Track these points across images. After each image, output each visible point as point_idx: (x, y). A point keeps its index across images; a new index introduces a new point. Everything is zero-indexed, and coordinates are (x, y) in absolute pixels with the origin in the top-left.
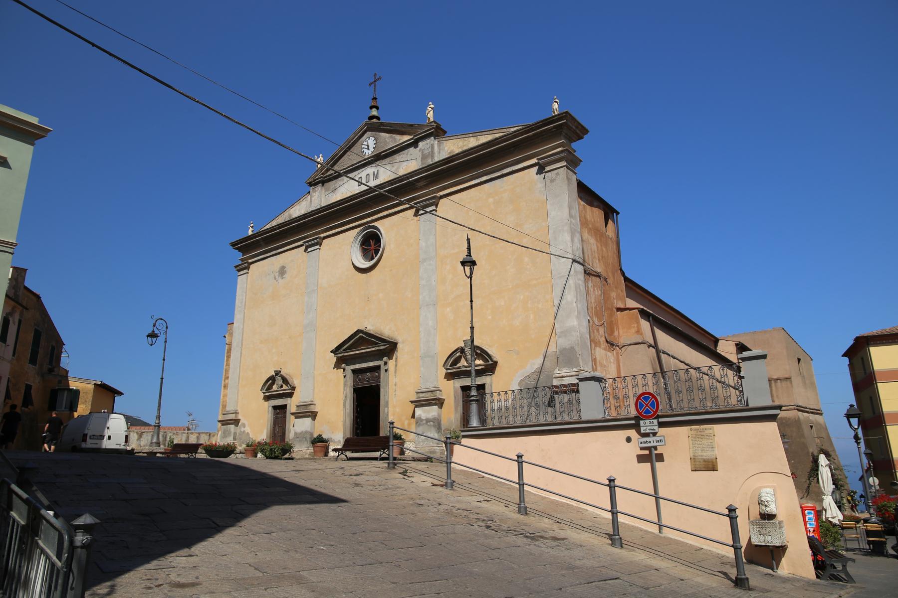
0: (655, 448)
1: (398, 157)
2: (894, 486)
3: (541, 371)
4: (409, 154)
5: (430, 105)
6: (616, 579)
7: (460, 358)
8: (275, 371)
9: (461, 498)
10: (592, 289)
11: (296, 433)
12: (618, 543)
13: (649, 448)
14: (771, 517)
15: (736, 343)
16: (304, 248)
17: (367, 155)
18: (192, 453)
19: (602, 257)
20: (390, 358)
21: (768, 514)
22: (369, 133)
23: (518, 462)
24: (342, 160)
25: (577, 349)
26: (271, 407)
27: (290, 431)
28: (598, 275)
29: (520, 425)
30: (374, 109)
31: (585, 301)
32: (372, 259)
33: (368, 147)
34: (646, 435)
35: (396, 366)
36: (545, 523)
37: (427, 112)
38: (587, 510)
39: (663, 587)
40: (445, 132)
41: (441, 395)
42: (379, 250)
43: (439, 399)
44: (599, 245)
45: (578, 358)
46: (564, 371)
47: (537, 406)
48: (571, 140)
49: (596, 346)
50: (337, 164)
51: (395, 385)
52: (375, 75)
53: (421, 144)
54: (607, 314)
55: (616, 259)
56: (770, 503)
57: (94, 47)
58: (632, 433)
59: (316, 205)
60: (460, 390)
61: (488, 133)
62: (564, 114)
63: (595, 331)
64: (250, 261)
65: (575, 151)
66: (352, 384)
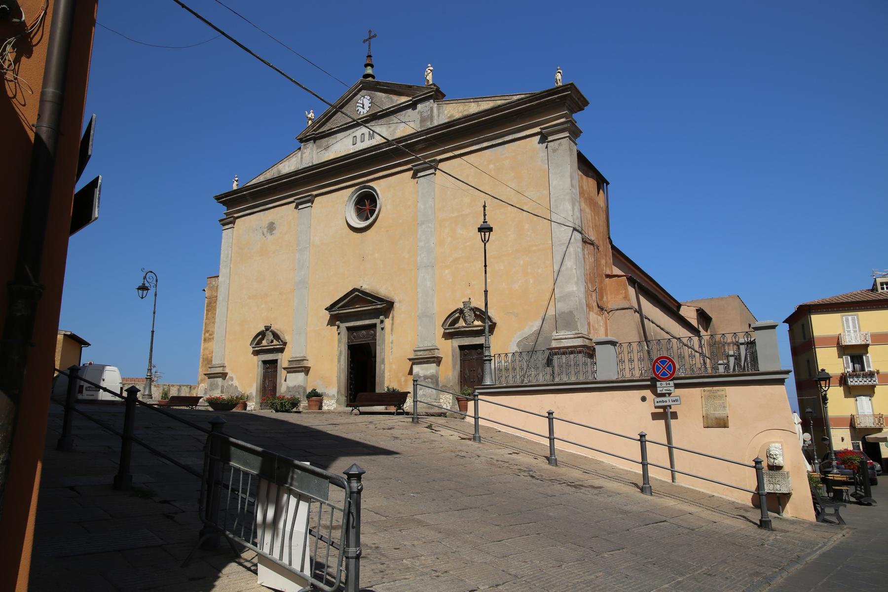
0: (670, 407)
1: (394, 119)
2: (825, 441)
3: (539, 332)
4: (407, 115)
5: (429, 67)
6: (664, 521)
7: (458, 318)
8: (265, 327)
9: (493, 450)
10: (587, 257)
11: (288, 388)
12: (648, 491)
13: (664, 407)
14: (779, 468)
15: (697, 308)
16: (294, 204)
17: (362, 113)
18: (192, 406)
19: (595, 226)
20: (387, 317)
21: (776, 466)
22: (363, 92)
23: (475, 419)
24: (335, 117)
25: (575, 313)
26: (261, 362)
27: (282, 385)
28: (592, 244)
29: (512, 385)
30: (369, 67)
31: (583, 269)
32: (367, 219)
33: (363, 106)
34: (663, 395)
35: (393, 324)
36: (576, 474)
37: (426, 74)
38: (603, 462)
39: (704, 528)
40: (444, 96)
41: (439, 353)
42: (375, 210)
43: (438, 358)
44: (593, 214)
45: (577, 322)
46: (562, 334)
47: (537, 368)
48: (573, 111)
49: (590, 311)
50: (330, 121)
51: (392, 343)
52: (370, 31)
53: (419, 106)
54: (599, 280)
55: (606, 228)
56: (778, 456)
57: (184, 8)
58: (647, 393)
59: (307, 163)
60: (458, 350)
61: (489, 99)
62: (569, 86)
63: (590, 297)
64: (236, 215)
65: (576, 122)
66: (347, 341)
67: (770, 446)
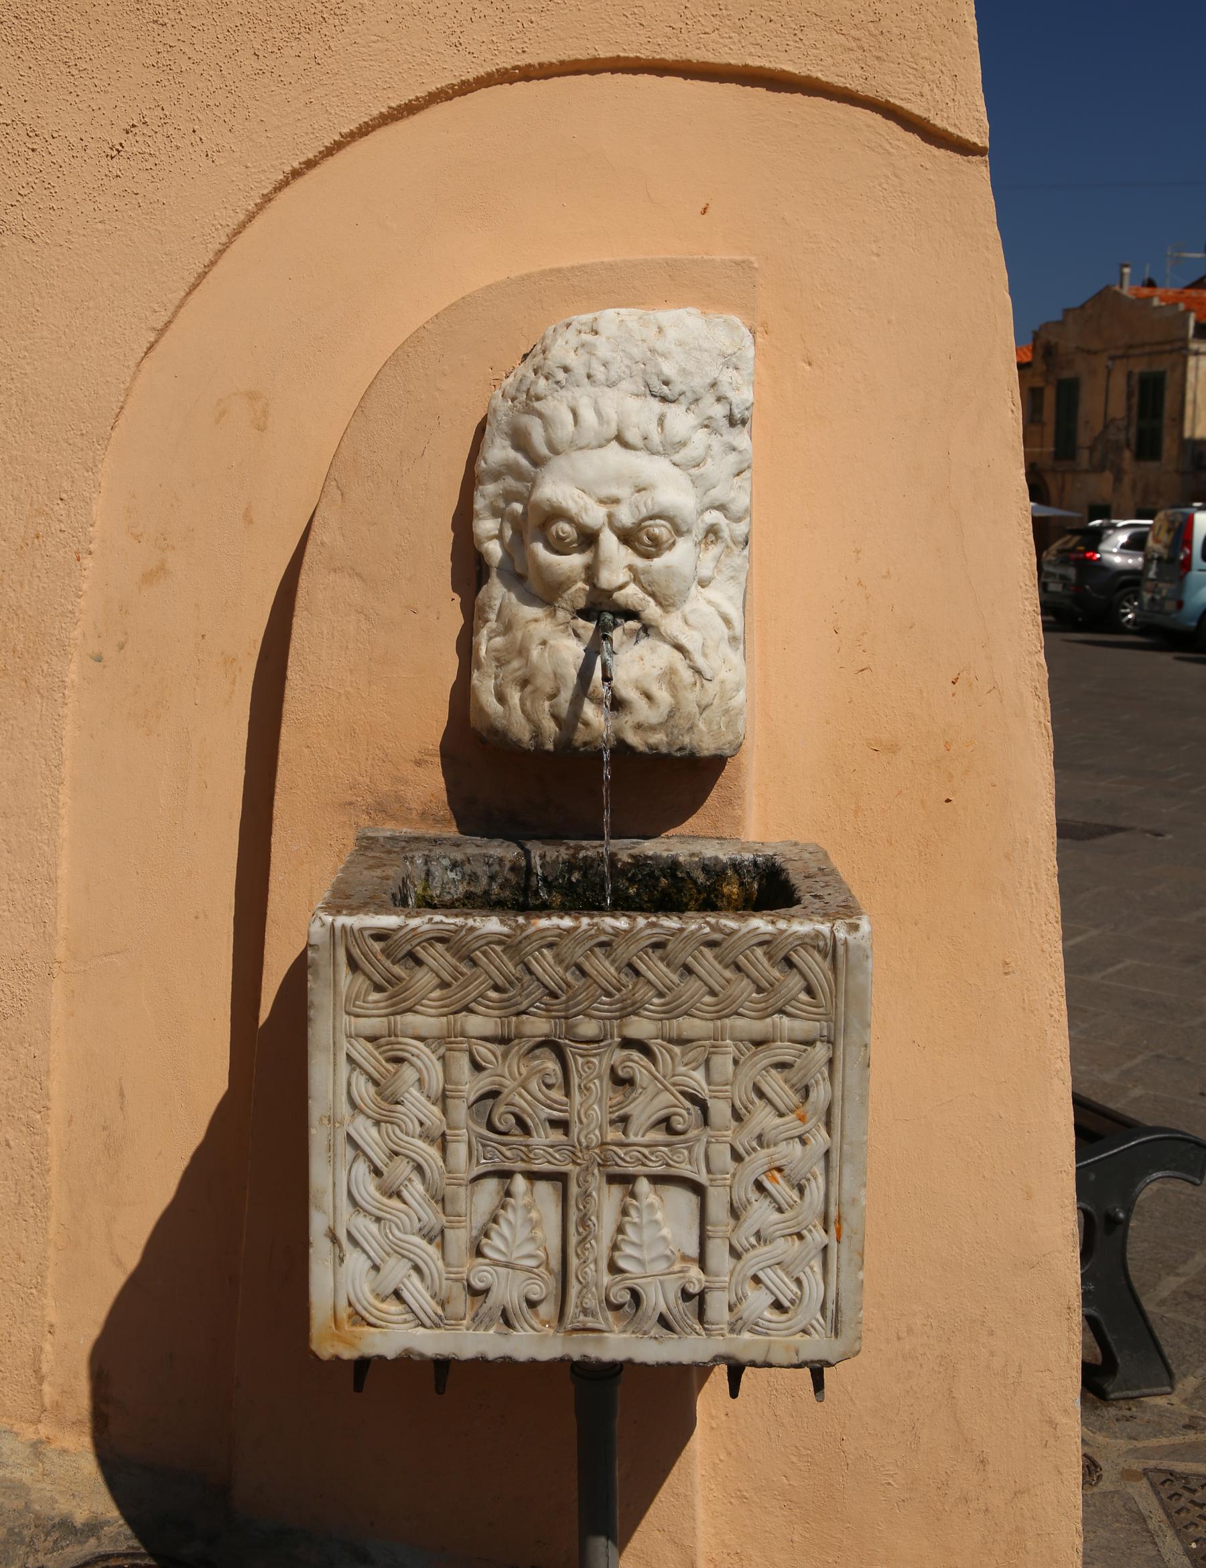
67: (563, 350)
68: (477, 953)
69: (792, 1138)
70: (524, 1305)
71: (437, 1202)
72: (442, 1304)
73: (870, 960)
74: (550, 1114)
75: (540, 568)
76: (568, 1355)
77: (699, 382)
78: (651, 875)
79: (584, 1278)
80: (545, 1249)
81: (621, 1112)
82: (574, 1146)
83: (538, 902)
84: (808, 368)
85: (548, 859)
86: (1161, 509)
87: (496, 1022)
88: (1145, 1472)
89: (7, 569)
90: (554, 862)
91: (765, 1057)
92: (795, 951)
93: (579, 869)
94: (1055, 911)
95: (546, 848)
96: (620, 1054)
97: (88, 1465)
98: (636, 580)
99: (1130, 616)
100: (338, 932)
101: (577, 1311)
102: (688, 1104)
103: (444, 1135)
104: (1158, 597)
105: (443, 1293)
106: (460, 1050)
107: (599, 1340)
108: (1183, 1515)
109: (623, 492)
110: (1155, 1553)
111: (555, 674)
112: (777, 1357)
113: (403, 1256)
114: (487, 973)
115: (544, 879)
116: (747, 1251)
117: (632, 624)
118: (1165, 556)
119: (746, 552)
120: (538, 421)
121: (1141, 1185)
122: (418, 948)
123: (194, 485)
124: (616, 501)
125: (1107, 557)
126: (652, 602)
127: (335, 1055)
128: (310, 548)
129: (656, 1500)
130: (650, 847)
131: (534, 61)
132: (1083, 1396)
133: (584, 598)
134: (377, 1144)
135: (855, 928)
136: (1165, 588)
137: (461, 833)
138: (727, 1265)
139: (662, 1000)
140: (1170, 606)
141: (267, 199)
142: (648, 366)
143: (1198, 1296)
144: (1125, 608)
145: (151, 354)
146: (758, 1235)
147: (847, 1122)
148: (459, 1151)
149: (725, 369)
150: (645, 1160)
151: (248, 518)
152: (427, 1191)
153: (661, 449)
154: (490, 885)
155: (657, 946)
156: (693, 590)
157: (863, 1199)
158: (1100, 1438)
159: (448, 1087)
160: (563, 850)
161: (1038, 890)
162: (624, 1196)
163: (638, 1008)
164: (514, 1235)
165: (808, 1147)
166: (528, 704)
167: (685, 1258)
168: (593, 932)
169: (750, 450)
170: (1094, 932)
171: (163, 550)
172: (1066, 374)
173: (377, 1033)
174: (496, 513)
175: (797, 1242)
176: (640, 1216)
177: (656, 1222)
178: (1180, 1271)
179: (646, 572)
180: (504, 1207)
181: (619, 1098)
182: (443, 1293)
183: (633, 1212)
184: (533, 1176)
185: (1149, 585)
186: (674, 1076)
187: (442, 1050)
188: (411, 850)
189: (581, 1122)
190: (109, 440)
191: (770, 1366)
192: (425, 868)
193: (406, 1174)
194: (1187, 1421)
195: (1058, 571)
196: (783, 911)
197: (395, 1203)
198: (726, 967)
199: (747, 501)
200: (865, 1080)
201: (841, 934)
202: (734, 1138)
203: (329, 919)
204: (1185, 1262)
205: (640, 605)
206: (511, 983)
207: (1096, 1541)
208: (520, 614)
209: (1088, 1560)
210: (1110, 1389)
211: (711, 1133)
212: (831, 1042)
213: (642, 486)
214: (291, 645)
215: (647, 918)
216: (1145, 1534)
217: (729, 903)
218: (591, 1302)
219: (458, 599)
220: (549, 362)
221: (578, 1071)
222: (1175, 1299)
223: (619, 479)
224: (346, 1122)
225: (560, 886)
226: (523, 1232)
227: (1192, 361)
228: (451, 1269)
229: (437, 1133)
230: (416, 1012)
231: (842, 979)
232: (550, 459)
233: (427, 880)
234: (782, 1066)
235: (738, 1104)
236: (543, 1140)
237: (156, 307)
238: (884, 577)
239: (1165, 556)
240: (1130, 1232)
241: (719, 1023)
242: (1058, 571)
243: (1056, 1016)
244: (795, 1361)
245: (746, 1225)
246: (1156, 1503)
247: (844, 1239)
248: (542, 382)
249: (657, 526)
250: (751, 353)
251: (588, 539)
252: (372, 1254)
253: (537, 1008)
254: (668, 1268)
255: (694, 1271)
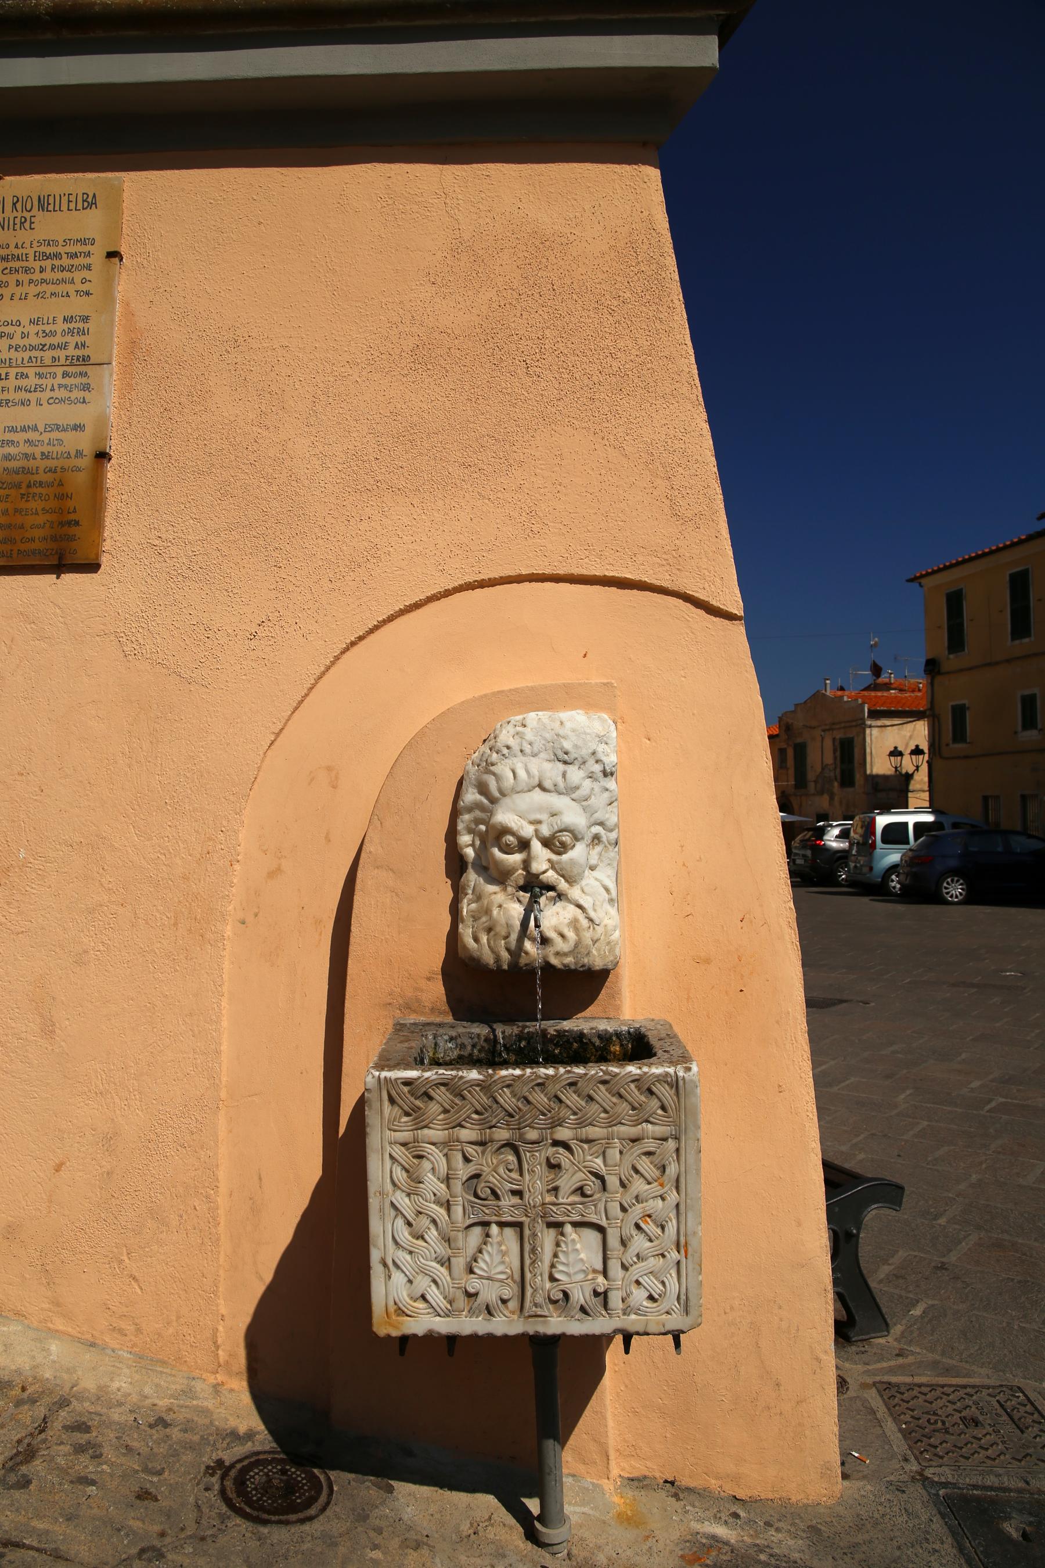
56: (578, 853)
67: (506, 736)
68: (465, 1091)
69: (656, 1197)
70: (499, 1302)
71: (445, 1241)
72: (451, 1303)
73: (698, 1088)
74: (511, 1187)
75: (497, 863)
76: (527, 1332)
77: (585, 752)
78: (568, 1041)
79: (534, 1285)
80: (511, 1268)
81: (554, 1185)
82: (526, 1206)
83: (501, 1060)
84: (648, 742)
85: (506, 1034)
86: (858, 814)
87: (477, 1133)
88: (874, 1384)
89: (191, 872)
90: (510, 1035)
91: (638, 1149)
92: (654, 1085)
93: (525, 1039)
94: (807, 1054)
95: (505, 1027)
96: (551, 1150)
97: (246, 1398)
98: (553, 868)
99: (843, 877)
100: (382, 1082)
101: (531, 1305)
102: (593, 1179)
103: (448, 1201)
104: (858, 865)
105: (451, 1296)
106: (457, 1150)
107: (545, 1322)
108: (897, 1408)
109: (543, 817)
110: (881, 1432)
111: (507, 924)
112: (651, 1329)
113: (426, 1274)
114: (471, 1104)
115: (505, 1046)
116: (632, 1265)
117: (551, 894)
118: (861, 842)
119: (616, 849)
120: (493, 778)
121: (865, 1213)
122: (430, 1090)
123: (296, 821)
124: (540, 822)
125: (828, 843)
126: (563, 880)
127: (382, 1154)
128: (363, 855)
129: (583, 1416)
130: (567, 1025)
131: (486, 577)
132: (836, 1341)
133: (523, 879)
134: (408, 1207)
135: (689, 1069)
136: (862, 860)
137: (455, 1020)
138: (620, 1274)
139: (576, 1117)
140: (865, 870)
141: (337, 658)
142: (555, 745)
143: (901, 1277)
144: (840, 872)
145: (272, 747)
146: (638, 1256)
147: (689, 1186)
148: (458, 1211)
149: (600, 744)
150: (568, 1213)
151: (328, 839)
152: (439, 1235)
153: (564, 791)
154: (472, 1050)
155: (572, 1084)
156: (586, 872)
157: (700, 1232)
158: (847, 1365)
159: (450, 1172)
160: (515, 1028)
161: (796, 1041)
162: (557, 1235)
163: (563, 1122)
164: (492, 1260)
165: (666, 1202)
166: (492, 942)
167: (595, 1271)
168: (533, 1077)
169: (616, 790)
170: (832, 1063)
171: (279, 858)
172: (799, 740)
173: (407, 1141)
174: (470, 831)
175: (661, 1259)
176: (567, 1247)
177: (577, 1250)
178: (890, 1262)
179: (559, 863)
180: (485, 1244)
181: (552, 1176)
182: (451, 1296)
183: (563, 1245)
184: (502, 1225)
185: (853, 858)
186: (584, 1162)
187: (445, 1151)
188: (425, 1031)
189: (530, 1191)
190: (248, 796)
191: (648, 1334)
192: (434, 1041)
193: (426, 1225)
194: (897, 1352)
195: (801, 852)
196: (646, 1061)
197: (420, 1242)
198: (613, 1095)
199: (616, 819)
200: (698, 1160)
201: (681, 1074)
202: (621, 1198)
203: (377, 1073)
204: (893, 1257)
205: (556, 882)
206: (486, 1109)
207: (847, 1427)
208: (486, 890)
209: (843, 1439)
210: (852, 1336)
211: (607, 1195)
212: (677, 1138)
213: (554, 813)
214: (353, 912)
215: (565, 1068)
216: (875, 1421)
217: (615, 1057)
218: (539, 1299)
219: (450, 882)
220: (498, 744)
221: (527, 1161)
222: (888, 1279)
223: (540, 809)
224: (390, 1195)
225: (514, 1050)
226: (497, 1259)
227: (868, 731)
228: (455, 1282)
229: (444, 1200)
230: (429, 1128)
231: (682, 1100)
232: (500, 799)
233: (435, 1048)
234: (649, 1154)
235: (623, 1177)
236: (508, 1203)
237: (275, 721)
238: (698, 861)
239: (861, 842)
240: (860, 1240)
241: (610, 1129)
242: (801, 852)
243: (811, 1116)
244: (663, 1331)
245: (630, 1250)
246: (881, 1402)
247: (689, 1256)
248: (495, 755)
249: (564, 836)
250: (614, 734)
251: (524, 845)
252: (408, 1273)
253: (501, 1123)
254: (586, 1277)
255: (601, 1279)
